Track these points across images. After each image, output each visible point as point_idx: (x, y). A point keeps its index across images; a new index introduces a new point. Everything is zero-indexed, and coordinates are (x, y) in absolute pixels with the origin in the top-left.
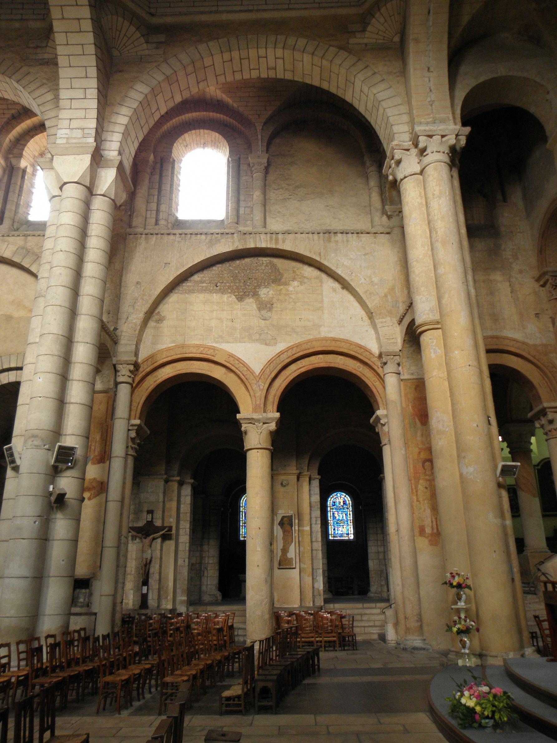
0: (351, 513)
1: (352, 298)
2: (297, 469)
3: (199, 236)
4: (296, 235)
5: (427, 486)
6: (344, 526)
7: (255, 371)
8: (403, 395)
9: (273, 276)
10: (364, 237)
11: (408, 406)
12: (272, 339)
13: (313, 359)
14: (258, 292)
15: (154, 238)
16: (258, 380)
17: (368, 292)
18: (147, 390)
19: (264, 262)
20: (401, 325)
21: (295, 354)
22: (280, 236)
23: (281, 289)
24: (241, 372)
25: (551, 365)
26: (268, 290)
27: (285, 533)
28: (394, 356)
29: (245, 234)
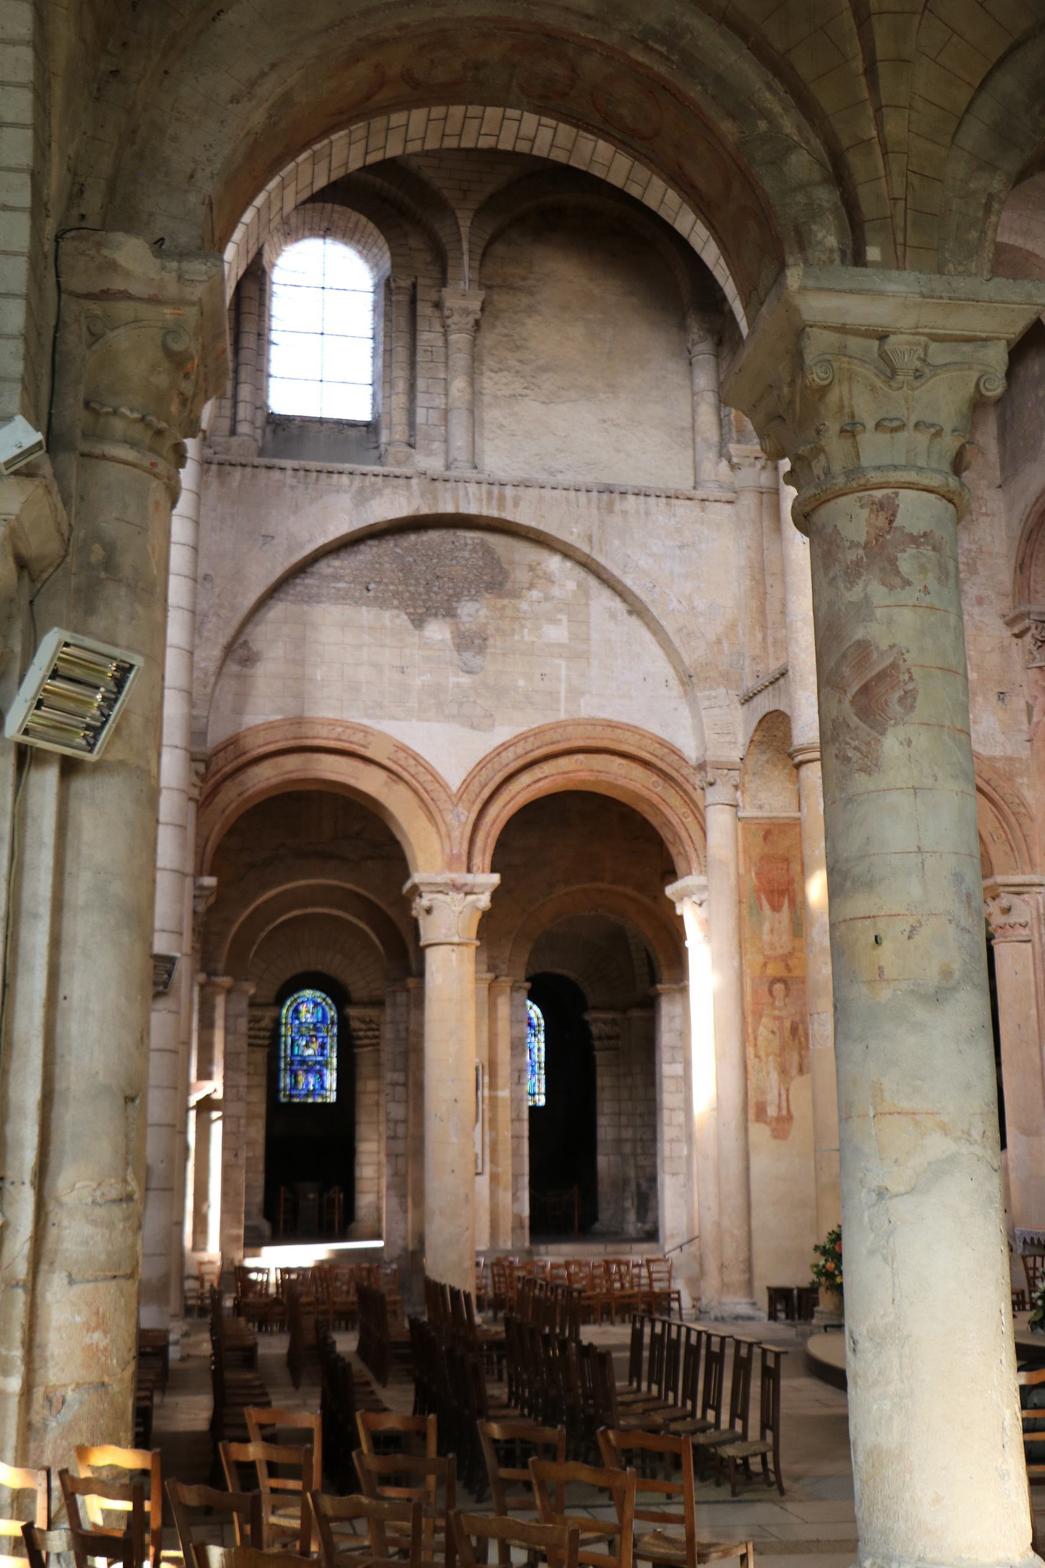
1: (647, 636)
3: (335, 476)
4: (543, 491)
7: (450, 784)
8: (741, 850)
9: (487, 574)
10: (681, 507)
11: (750, 871)
13: (564, 763)
14: (456, 608)
15: (238, 473)
17: (685, 631)
18: (223, 812)
19: (469, 541)
20: (746, 706)
21: (532, 750)
22: (509, 491)
23: (504, 607)
25: (1017, 801)
26: (477, 605)
29: (434, 480)
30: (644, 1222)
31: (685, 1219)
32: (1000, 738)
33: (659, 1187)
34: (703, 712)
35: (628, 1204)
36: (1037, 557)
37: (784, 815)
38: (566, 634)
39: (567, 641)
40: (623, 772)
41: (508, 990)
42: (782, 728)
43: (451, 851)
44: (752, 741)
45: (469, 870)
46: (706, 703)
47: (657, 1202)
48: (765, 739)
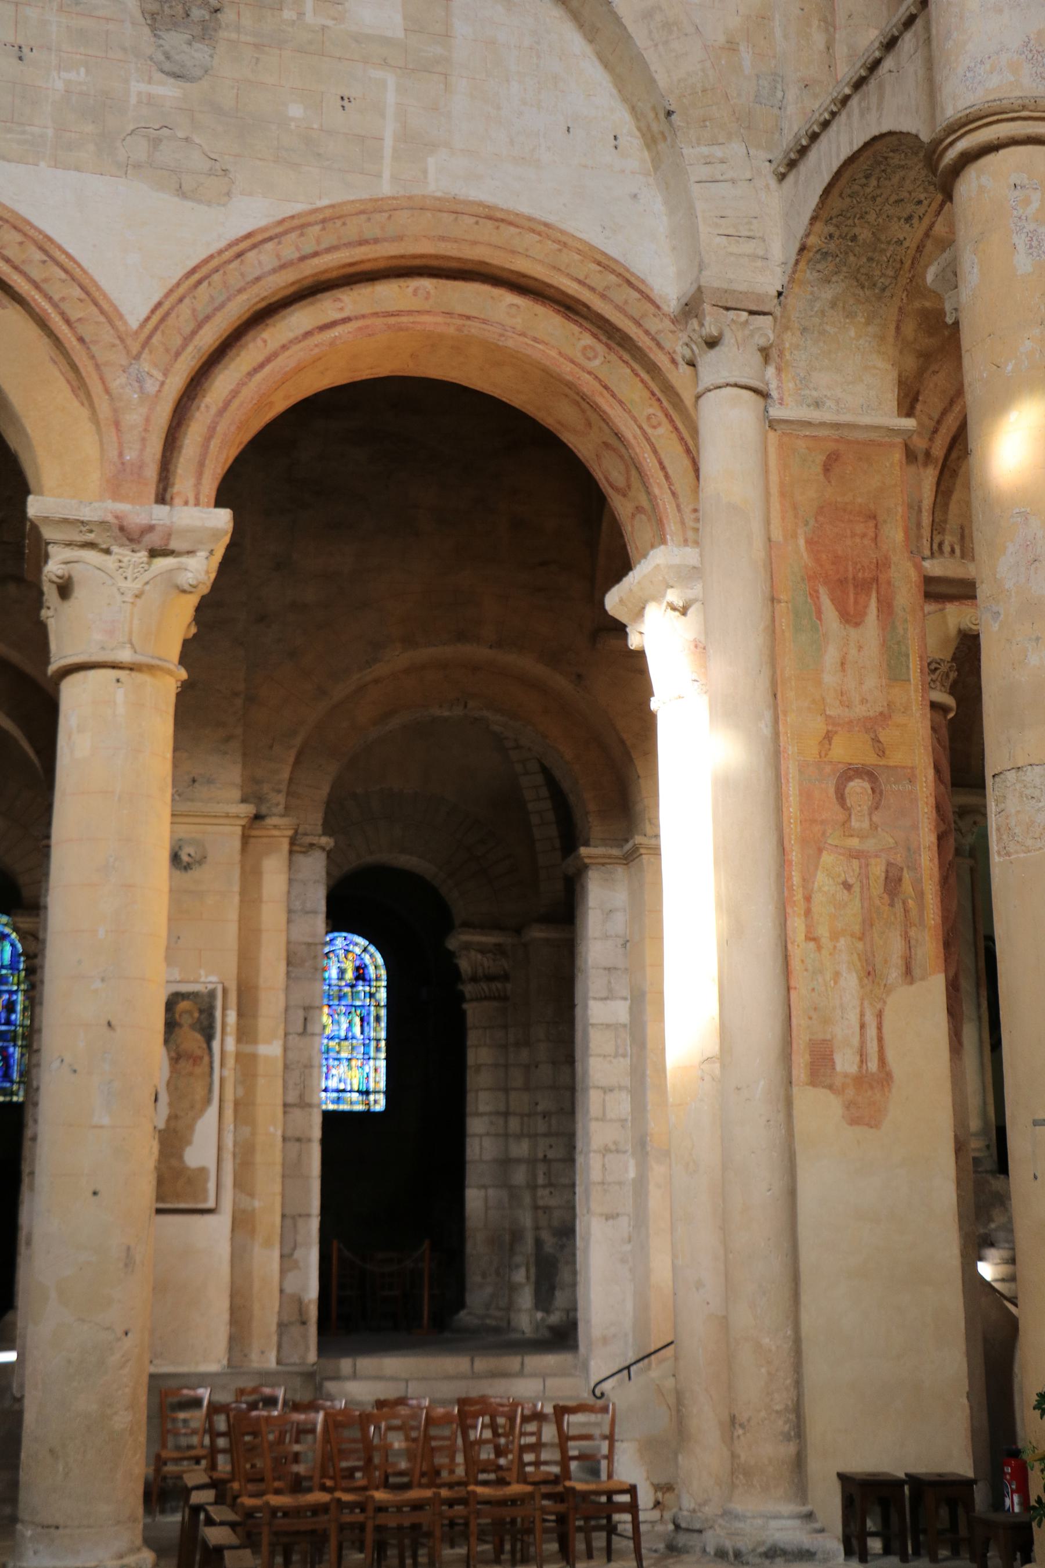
0: (383, 1012)
2: (244, 800)
5: (851, 881)
6: (354, 1063)
8: (774, 490)
11: (794, 536)
12: (211, 173)
16: (135, 348)
21: (316, 254)
24: (55, 306)
27: (182, 1063)
28: (752, 313)
30: (547, 1311)
31: (629, 1306)
33: (579, 1243)
34: (696, 189)
35: (519, 1276)
37: (866, 420)
38: (398, 19)
39: (400, 34)
40: (518, 322)
41: (286, 847)
42: (871, 217)
43: (121, 455)
44: (803, 249)
45: (162, 498)
46: (704, 172)
47: (574, 1273)
48: (832, 246)
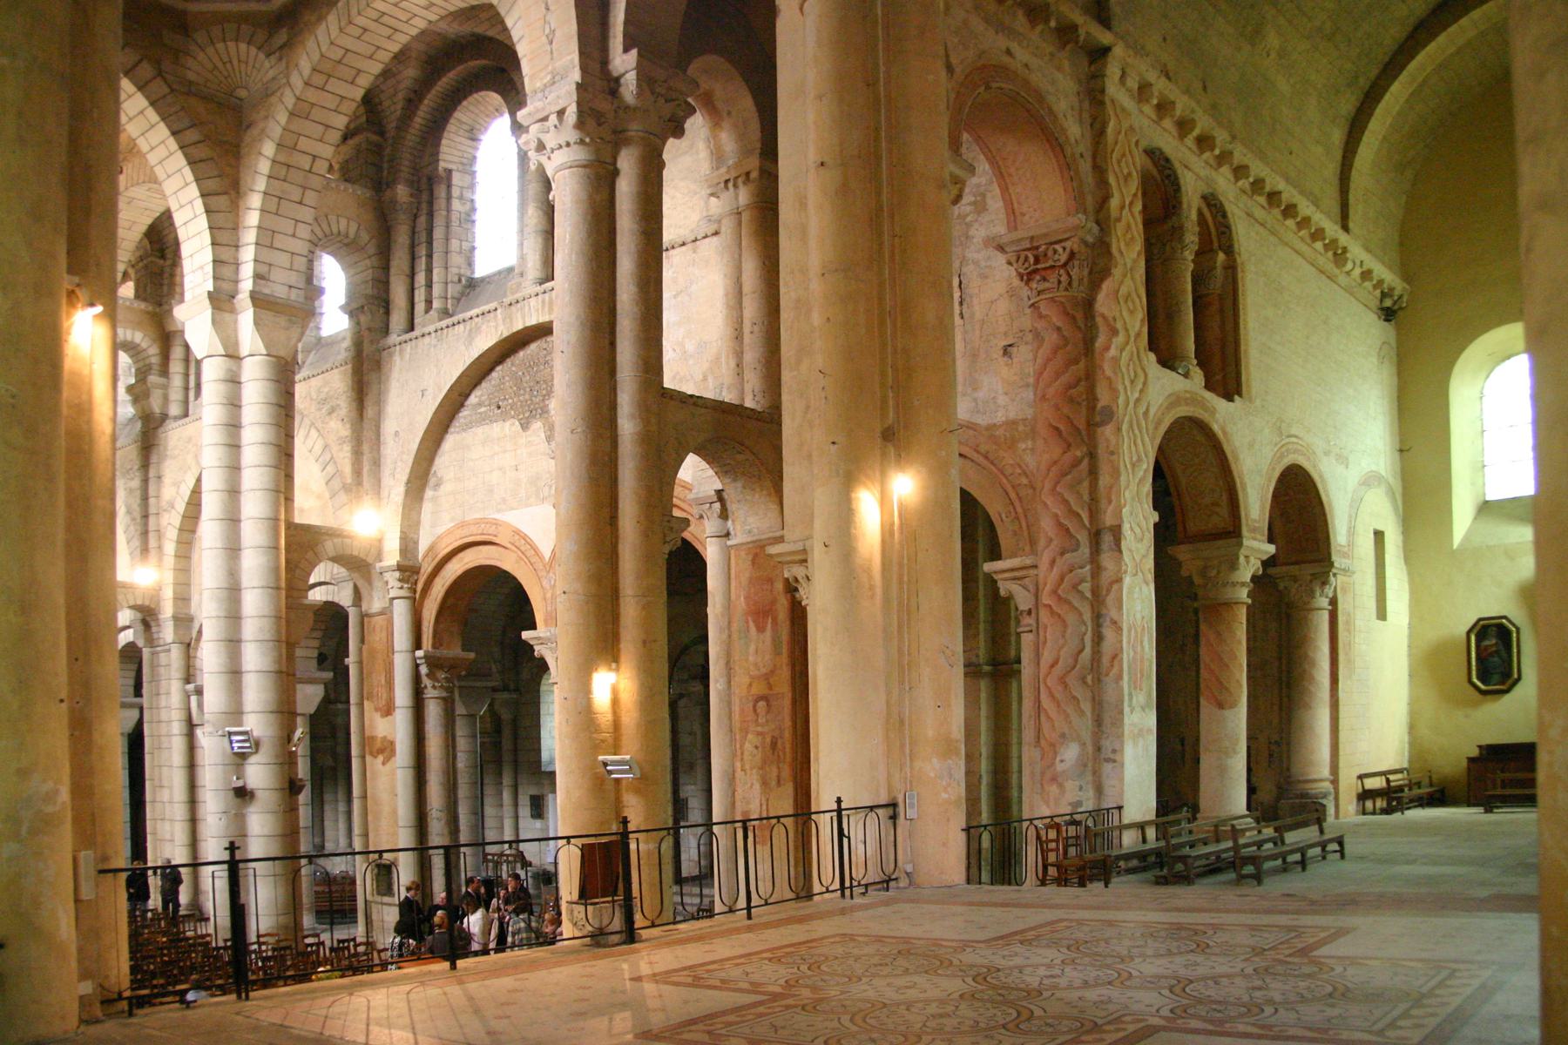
32: (1002, 400)
36: (1010, 175)
